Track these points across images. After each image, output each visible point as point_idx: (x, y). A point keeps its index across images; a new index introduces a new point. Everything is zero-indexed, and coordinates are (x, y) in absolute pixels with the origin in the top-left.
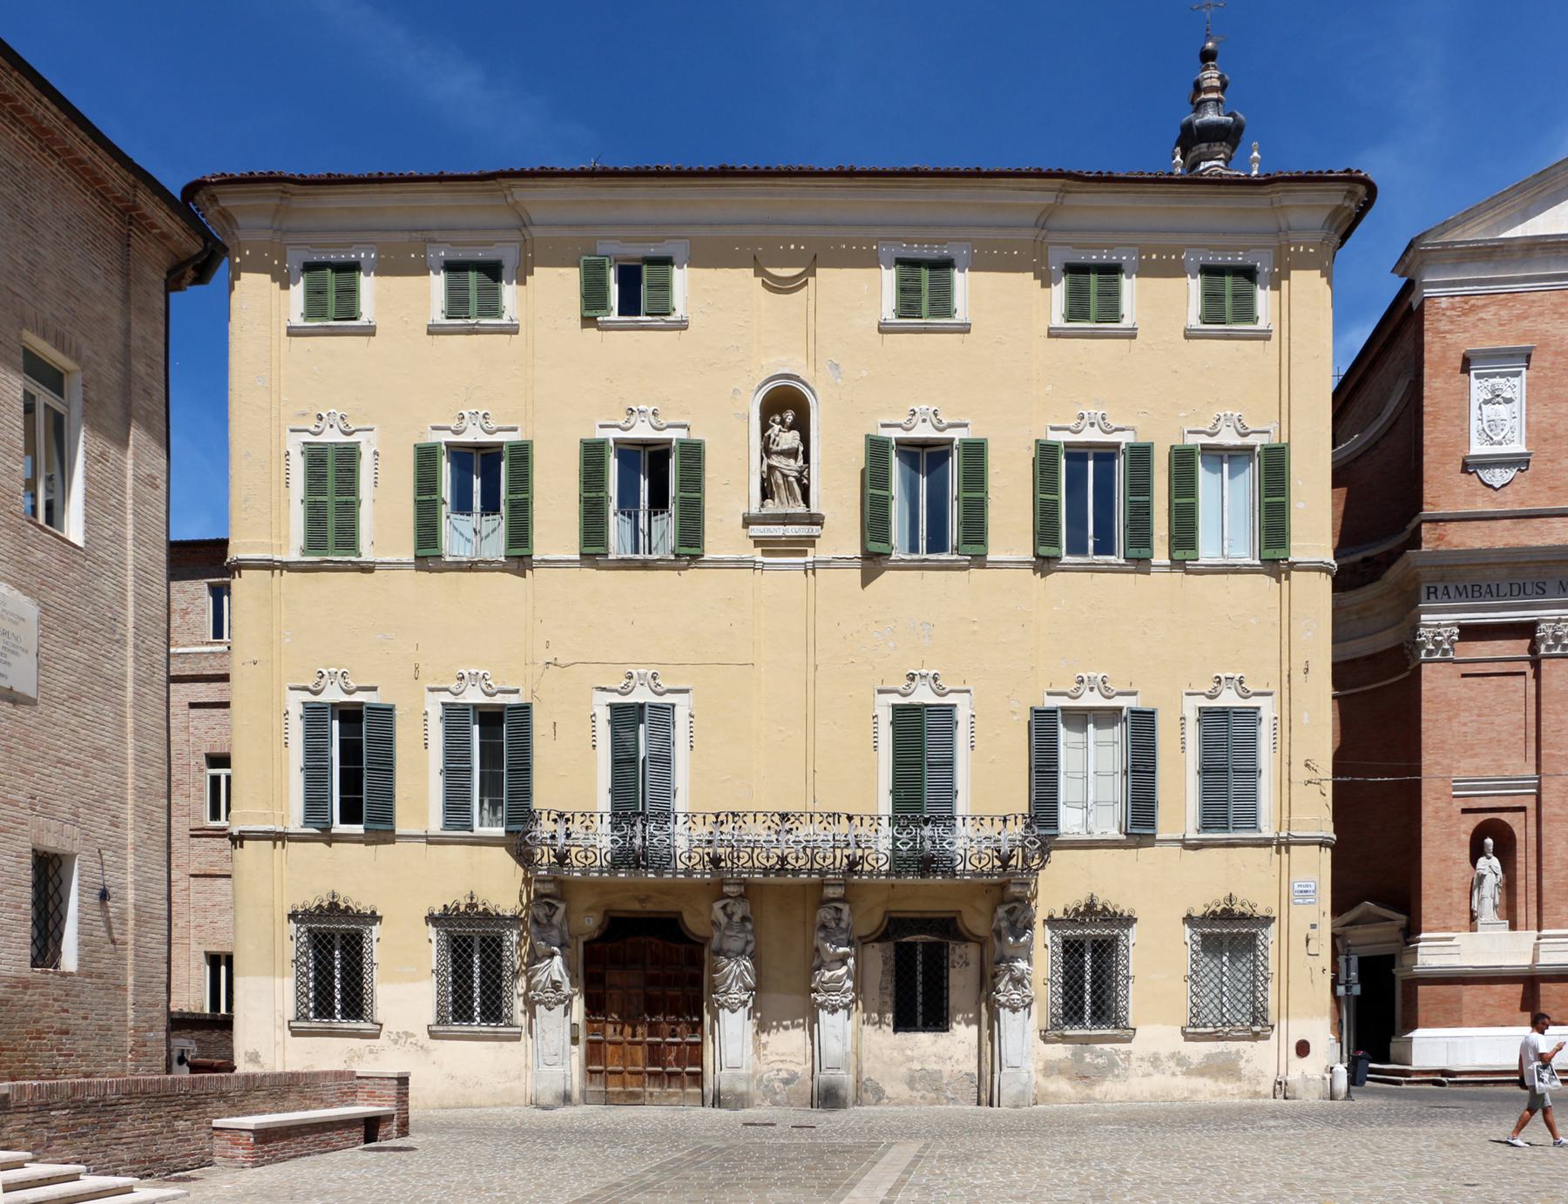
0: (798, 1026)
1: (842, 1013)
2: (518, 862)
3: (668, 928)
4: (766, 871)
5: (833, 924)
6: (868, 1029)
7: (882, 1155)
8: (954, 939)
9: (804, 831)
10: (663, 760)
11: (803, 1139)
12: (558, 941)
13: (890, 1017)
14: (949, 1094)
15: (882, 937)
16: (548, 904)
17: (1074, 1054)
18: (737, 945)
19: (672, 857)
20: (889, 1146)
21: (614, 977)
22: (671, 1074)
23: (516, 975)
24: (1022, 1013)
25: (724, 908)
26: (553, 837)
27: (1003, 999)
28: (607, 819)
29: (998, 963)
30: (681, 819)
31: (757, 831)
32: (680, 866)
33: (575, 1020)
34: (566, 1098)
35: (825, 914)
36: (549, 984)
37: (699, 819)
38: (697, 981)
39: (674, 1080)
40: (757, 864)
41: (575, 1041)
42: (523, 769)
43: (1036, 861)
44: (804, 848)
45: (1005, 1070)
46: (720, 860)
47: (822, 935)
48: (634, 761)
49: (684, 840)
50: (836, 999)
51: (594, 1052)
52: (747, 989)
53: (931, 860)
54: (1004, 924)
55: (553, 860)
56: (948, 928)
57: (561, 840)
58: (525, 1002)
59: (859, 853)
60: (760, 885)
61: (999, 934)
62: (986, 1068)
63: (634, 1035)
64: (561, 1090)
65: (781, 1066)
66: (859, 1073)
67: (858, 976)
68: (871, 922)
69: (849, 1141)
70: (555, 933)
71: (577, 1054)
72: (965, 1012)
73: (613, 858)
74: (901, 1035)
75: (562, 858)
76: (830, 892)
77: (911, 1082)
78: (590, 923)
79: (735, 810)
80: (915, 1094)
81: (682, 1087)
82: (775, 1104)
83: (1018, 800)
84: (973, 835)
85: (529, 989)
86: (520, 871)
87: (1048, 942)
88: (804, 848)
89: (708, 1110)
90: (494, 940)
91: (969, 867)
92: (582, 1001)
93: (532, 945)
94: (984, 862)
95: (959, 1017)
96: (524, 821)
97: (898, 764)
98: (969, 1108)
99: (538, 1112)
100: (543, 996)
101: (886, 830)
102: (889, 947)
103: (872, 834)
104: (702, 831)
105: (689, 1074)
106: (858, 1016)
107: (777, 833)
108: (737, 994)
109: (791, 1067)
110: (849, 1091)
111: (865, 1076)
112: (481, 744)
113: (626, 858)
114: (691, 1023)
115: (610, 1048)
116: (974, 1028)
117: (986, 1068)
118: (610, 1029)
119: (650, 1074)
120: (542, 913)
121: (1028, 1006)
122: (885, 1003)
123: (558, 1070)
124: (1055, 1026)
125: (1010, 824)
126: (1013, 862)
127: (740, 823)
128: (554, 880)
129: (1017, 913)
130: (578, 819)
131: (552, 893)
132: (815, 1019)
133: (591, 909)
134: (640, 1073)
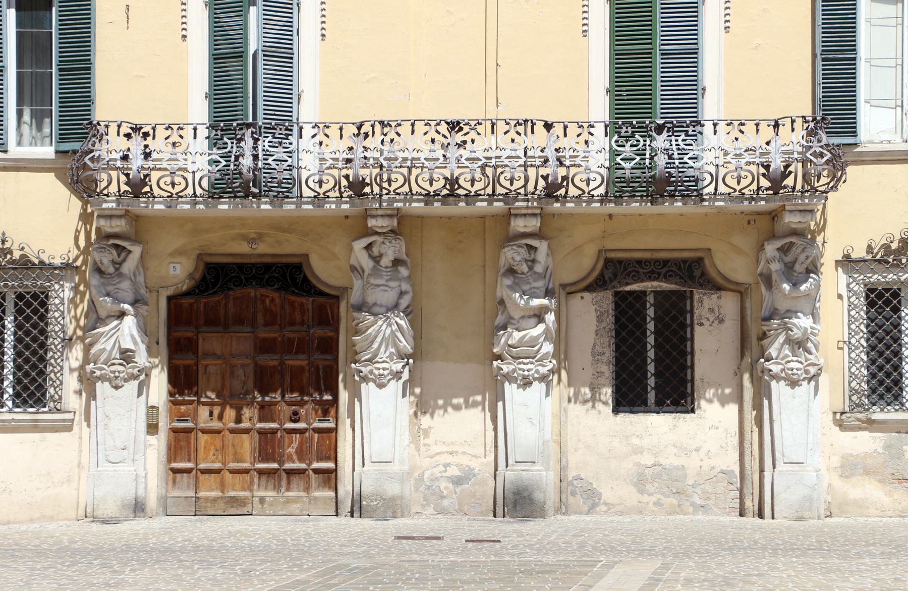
0: (475, 404)
1: (538, 388)
2: (74, 191)
3: (290, 276)
4: (429, 198)
5: (525, 268)
6: (576, 409)
7: (600, 576)
8: (701, 286)
9: (483, 145)
10: (282, 53)
11: (482, 555)
12: (130, 296)
13: (607, 392)
14: (697, 500)
15: (596, 285)
16: (116, 246)
17: (888, 447)
18: (386, 297)
19: (295, 182)
20: (610, 565)
21: (211, 342)
22: (290, 473)
23: (68, 342)
24: (805, 388)
25: (369, 247)
26: (125, 158)
27: (775, 369)
28: (203, 132)
29: (767, 319)
30: (308, 131)
31: (416, 145)
32: (307, 192)
33: (153, 401)
34: (138, 508)
35: (513, 255)
36: (116, 354)
37: (334, 131)
38: (330, 346)
39: (295, 479)
40: (415, 188)
41: (152, 428)
42: (79, 68)
43: (824, 180)
44: (483, 168)
45: (780, 466)
46: (363, 184)
47: (508, 281)
48: (240, 56)
49: (313, 159)
50: (529, 368)
51: (180, 442)
52: (401, 356)
53: (667, 180)
54: (775, 266)
55: (124, 188)
56: (692, 272)
57: (137, 161)
58: (81, 379)
59: (562, 172)
60: (421, 218)
61: (768, 280)
62: (752, 465)
63: (238, 420)
64: (131, 496)
65: (448, 459)
66: (563, 470)
67: (561, 339)
68: (584, 263)
69: (551, 559)
70: (126, 285)
71: (158, 445)
72: (719, 386)
73: (212, 185)
74: (625, 418)
75: (138, 187)
76: (519, 225)
77: (640, 482)
78: (178, 272)
79: (385, 118)
80: (646, 498)
81: (307, 489)
82: (442, 511)
83: (798, 98)
84: (729, 147)
85: (86, 360)
86: (77, 204)
87: (844, 292)
88: (483, 168)
89: (344, 520)
90: (35, 296)
91: (722, 189)
92: (164, 376)
93: (92, 302)
94: (744, 183)
95: (710, 393)
96: (83, 137)
97: (618, 57)
98: (726, 519)
99: (96, 527)
100: (108, 370)
101: (601, 141)
102: (606, 298)
103: (581, 147)
104: (337, 146)
105: (317, 471)
106: (560, 390)
107: (445, 147)
108: (387, 362)
109: (465, 461)
110: (548, 493)
111: (572, 474)
112: (20, 36)
113: (228, 184)
114: (321, 403)
115: (203, 438)
116: (733, 408)
117: (752, 465)
118: (204, 412)
119: (261, 472)
120: (106, 259)
121: (814, 377)
122: (600, 374)
123: (127, 469)
124: (856, 407)
125: (784, 130)
126: (789, 182)
127: (392, 135)
128: (127, 214)
129: (794, 251)
130: (161, 133)
131: (119, 235)
132: (499, 396)
133: (180, 252)
134: (246, 471)
